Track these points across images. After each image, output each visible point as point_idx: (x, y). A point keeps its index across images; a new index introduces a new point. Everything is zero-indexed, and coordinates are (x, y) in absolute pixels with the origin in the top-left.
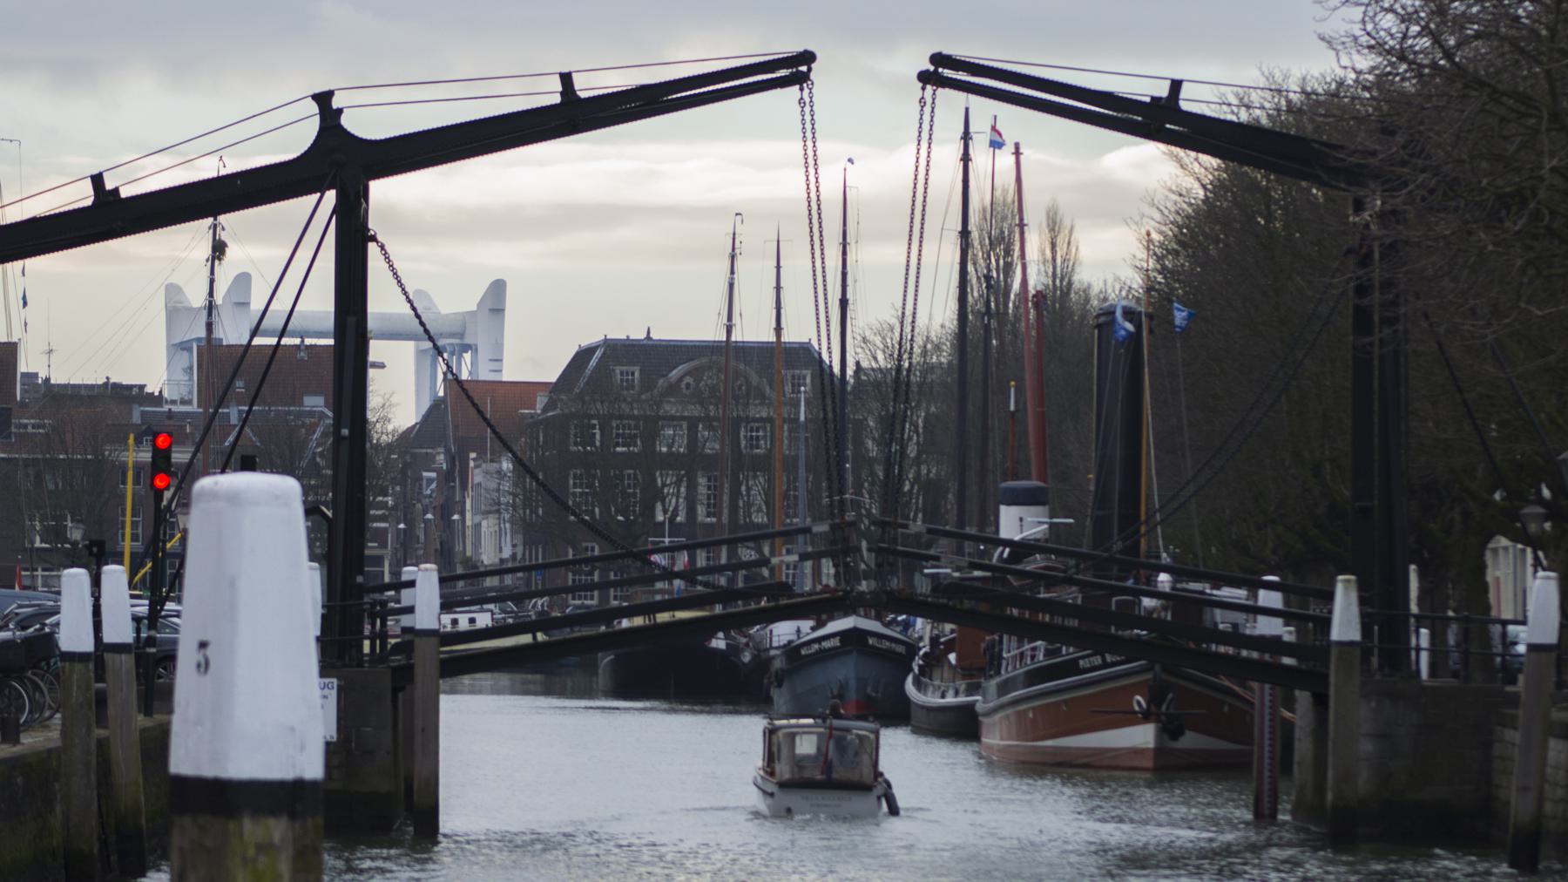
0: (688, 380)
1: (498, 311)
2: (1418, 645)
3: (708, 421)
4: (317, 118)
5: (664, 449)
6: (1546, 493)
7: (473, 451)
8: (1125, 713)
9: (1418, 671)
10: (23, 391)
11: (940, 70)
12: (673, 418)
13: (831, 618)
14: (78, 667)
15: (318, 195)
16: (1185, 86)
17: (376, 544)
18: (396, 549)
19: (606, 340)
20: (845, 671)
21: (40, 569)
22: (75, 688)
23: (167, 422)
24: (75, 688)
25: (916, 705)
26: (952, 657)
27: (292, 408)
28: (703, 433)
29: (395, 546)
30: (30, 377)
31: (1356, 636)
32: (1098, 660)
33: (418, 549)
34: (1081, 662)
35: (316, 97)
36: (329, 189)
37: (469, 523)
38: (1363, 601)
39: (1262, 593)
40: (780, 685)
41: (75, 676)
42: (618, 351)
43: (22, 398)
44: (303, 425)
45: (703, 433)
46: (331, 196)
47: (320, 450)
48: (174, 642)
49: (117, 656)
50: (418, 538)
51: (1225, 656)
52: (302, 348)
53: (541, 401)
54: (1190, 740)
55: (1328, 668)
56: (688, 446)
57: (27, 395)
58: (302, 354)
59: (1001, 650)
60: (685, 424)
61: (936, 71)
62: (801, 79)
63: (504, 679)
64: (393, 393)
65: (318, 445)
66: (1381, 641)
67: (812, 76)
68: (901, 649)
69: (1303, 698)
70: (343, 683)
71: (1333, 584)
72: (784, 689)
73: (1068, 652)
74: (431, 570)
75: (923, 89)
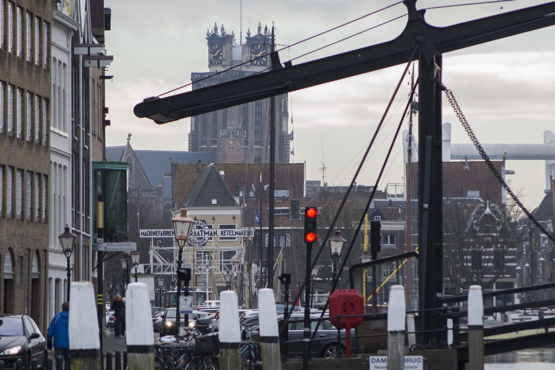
4: (407, 17)
7: (214, 198)
10: (308, 191)
14: (231, 351)
15: (406, 64)
17: (509, 276)
18: (527, 278)
21: (317, 292)
22: (229, 365)
23: (389, 207)
24: (229, 365)
27: (459, 198)
29: (527, 277)
30: (313, 184)
33: (539, 278)
36: (414, 59)
41: (229, 358)
43: (307, 195)
44: (466, 207)
46: (416, 64)
47: (475, 221)
49: (268, 344)
50: (539, 272)
52: (466, 163)
57: (310, 193)
58: (466, 167)
63: (535, 352)
64: (523, 189)
65: (475, 219)
70: (426, 359)
74: (478, 289)
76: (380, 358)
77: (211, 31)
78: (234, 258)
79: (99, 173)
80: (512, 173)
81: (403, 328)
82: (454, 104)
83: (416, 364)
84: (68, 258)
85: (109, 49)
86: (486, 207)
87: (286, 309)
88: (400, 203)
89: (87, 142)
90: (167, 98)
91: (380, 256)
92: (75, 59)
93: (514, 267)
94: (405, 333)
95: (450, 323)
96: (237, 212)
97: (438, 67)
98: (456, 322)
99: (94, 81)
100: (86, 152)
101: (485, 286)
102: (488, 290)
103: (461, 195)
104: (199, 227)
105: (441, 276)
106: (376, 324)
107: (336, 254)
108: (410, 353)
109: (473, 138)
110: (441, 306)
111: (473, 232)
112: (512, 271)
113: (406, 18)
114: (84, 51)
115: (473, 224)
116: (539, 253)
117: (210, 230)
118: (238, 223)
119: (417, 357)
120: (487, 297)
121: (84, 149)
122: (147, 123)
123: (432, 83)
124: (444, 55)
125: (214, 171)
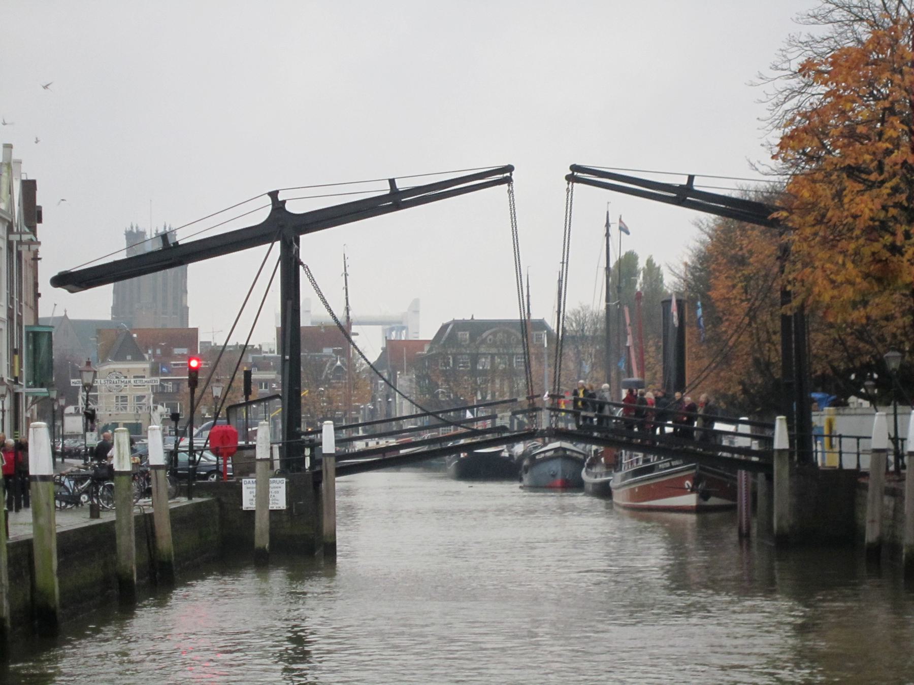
0: (491, 337)
1: (417, 312)
2: (816, 450)
3: (499, 355)
5: (481, 368)
6: (876, 376)
8: (680, 488)
9: (817, 463)
11: (575, 173)
12: (484, 354)
13: (550, 442)
15: (270, 244)
16: (696, 178)
19: (454, 320)
20: (556, 467)
25: (588, 483)
26: (603, 459)
28: (497, 360)
31: (786, 446)
32: (668, 465)
34: (660, 466)
35: (271, 194)
37: (397, 402)
38: (790, 429)
39: (740, 426)
40: (526, 473)
42: (459, 325)
45: (497, 360)
46: (278, 245)
48: (336, 446)
51: (726, 458)
53: (427, 348)
54: (713, 501)
55: (773, 461)
56: (491, 367)
59: (622, 459)
60: (489, 357)
61: (573, 174)
62: (508, 181)
66: (798, 449)
67: (513, 177)
68: (581, 457)
69: (761, 476)
71: (774, 421)
72: (528, 474)
73: (653, 459)
75: (568, 184)
76: (251, 480)
77: (129, 229)
78: (144, 401)
79: (31, 335)
80: (357, 334)
81: (268, 456)
82: (308, 273)
83: (280, 485)
84: (3, 402)
85: (40, 237)
86: (337, 361)
87: (176, 441)
88: (272, 357)
89: (21, 310)
90: (77, 272)
91: (251, 398)
92: (10, 244)
93: (359, 406)
94: (271, 460)
95: (307, 452)
96: (147, 366)
97: (296, 246)
98: (312, 451)
99: (26, 261)
100: (20, 318)
101: (335, 420)
102: (339, 424)
103: (319, 352)
104: (117, 378)
105: (300, 415)
106: (247, 453)
107: (217, 397)
108: (275, 476)
109: (330, 310)
110: (300, 438)
111: (327, 380)
112: (357, 409)
113: (270, 207)
114: (17, 237)
115: (327, 373)
116: (377, 396)
117: (125, 380)
118: (147, 374)
119: (281, 479)
120: (337, 429)
121: (18, 315)
122: (62, 291)
123: (291, 259)
124: (301, 237)
125: (129, 335)
